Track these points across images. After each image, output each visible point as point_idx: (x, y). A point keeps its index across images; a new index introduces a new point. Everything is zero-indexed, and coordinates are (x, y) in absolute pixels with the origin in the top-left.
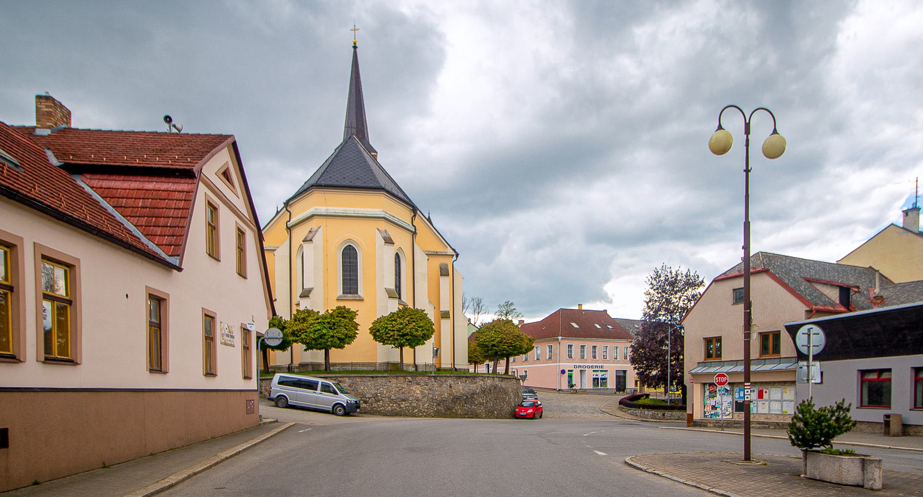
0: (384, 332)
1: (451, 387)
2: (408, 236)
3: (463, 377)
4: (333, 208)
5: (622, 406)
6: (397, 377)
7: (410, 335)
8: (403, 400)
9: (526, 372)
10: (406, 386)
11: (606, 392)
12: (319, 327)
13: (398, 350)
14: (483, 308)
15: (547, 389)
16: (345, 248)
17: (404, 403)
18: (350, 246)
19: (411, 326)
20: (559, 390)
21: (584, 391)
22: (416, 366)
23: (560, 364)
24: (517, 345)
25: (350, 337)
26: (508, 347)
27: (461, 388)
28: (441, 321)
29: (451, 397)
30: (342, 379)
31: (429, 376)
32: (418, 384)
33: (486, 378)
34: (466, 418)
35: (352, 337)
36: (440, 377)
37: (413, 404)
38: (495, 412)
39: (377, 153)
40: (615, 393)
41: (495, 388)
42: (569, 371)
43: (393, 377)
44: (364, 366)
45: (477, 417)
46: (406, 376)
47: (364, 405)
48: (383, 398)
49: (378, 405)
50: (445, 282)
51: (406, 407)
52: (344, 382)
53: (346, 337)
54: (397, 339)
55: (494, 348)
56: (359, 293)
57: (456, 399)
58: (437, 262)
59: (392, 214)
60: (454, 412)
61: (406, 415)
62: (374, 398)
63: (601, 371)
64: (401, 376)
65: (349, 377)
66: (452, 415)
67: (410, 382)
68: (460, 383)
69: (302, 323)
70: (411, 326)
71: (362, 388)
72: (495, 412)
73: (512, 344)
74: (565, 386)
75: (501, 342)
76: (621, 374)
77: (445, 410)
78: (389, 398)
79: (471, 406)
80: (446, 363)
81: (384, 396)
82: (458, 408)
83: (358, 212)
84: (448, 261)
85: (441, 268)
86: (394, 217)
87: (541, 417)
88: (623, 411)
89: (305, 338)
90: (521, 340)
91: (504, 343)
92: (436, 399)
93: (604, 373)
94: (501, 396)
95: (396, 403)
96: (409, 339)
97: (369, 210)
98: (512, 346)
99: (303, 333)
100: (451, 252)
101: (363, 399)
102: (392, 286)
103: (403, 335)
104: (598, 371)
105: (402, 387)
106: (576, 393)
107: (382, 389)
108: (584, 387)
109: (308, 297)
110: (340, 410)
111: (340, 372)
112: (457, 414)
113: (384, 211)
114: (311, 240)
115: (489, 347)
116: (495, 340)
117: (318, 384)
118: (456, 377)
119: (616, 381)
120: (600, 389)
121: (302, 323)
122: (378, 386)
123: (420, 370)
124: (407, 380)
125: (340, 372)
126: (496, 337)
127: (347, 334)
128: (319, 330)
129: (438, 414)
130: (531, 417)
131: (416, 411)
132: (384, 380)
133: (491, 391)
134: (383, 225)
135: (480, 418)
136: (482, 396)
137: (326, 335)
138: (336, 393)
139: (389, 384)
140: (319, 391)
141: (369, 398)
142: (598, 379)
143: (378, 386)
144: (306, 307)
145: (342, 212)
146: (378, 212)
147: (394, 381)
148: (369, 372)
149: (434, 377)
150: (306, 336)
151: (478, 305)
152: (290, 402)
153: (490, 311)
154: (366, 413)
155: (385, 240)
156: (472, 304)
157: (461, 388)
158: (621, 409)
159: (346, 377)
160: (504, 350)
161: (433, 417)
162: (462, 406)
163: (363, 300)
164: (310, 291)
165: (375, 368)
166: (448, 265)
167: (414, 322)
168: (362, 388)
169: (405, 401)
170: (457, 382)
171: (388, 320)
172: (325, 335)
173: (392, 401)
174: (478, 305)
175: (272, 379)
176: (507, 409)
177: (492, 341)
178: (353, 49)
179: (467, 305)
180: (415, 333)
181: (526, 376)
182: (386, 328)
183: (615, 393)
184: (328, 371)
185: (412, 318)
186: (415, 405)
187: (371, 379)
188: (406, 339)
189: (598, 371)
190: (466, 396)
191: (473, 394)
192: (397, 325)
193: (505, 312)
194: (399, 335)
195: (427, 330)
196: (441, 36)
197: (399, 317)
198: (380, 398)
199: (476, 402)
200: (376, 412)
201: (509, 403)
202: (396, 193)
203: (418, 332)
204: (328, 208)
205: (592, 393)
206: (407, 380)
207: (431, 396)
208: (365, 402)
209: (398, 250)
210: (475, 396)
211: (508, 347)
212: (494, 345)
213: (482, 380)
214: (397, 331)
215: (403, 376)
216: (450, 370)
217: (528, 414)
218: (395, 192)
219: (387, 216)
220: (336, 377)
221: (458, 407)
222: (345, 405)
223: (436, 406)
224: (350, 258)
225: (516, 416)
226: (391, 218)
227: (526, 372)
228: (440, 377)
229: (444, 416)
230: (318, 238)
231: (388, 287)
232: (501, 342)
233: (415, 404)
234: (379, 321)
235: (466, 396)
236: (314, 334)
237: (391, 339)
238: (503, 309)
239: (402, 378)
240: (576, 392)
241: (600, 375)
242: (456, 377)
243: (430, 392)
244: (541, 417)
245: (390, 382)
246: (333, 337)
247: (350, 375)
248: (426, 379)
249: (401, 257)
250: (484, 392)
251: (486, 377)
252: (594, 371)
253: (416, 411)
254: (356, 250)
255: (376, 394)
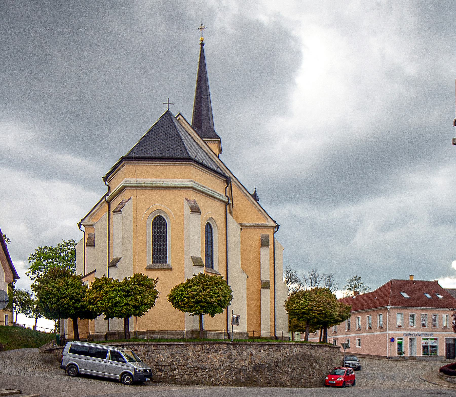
0: (180, 299)
1: (252, 355)
2: (221, 208)
3: (266, 345)
4: (143, 179)
5: (442, 374)
6: (194, 345)
7: (205, 302)
8: (200, 369)
9: (348, 341)
10: (202, 354)
11: (436, 359)
12: (112, 295)
13: (198, 317)
14: (334, 283)
15: (377, 356)
16: (155, 218)
17: (200, 371)
18: (159, 216)
19: (205, 292)
20: (389, 358)
21: (413, 359)
22: (228, 335)
23: (390, 332)
24: (327, 312)
25: (146, 304)
26: (318, 314)
27: (263, 356)
28: (262, 290)
29: (252, 365)
30: (138, 347)
31: (228, 344)
32: (216, 352)
33: (293, 346)
34: (268, 386)
35: (152, 304)
36: (240, 344)
37: (210, 372)
38: (303, 380)
39: (220, 138)
40: (445, 360)
41: (303, 355)
42: (399, 339)
43: (190, 345)
44: (172, 334)
45: (281, 385)
46: (203, 344)
47: (159, 374)
48: (179, 367)
49: (174, 373)
50: (266, 253)
51: (203, 375)
52: (140, 350)
53: (142, 305)
54: (192, 307)
55: (305, 316)
56: (168, 263)
57: (258, 367)
58: (257, 234)
59: (202, 185)
60: (255, 381)
61: (203, 384)
62: (170, 366)
63: (431, 339)
64: (198, 344)
65: (145, 345)
66: (253, 384)
67: (208, 350)
68: (262, 351)
69: (99, 290)
70: (205, 292)
71: (158, 356)
72: (303, 380)
73: (322, 311)
74: (395, 354)
75: (311, 310)
76: (451, 342)
77: (245, 379)
78: (186, 366)
79: (275, 374)
80: (266, 332)
81: (181, 364)
82: (260, 377)
83: (167, 183)
84: (269, 232)
85: (262, 239)
86: (204, 187)
87: (353, 385)
88: (443, 379)
89: (99, 306)
90: (331, 307)
91: (315, 310)
92: (236, 368)
93: (434, 341)
94: (311, 364)
95: (192, 371)
96: (204, 307)
97: (177, 180)
98: (322, 313)
99: (98, 301)
100: (271, 224)
101: (158, 367)
102: (200, 254)
103: (198, 302)
104: (427, 339)
105: (199, 355)
106: (404, 360)
107: (178, 357)
108: (413, 355)
109: (116, 266)
110: (128, 380)
111: (148, 340)
112: (258, 382)
113: (192, 181)
114: (120, 211)
115: (299, 314)
116: (305, 307)
117: (107, 352)
118: (258, 345)
119: (447, 349)
120: (430, 356)
121: (99, 290)
122: (174, 354)
123: (233, 337)
124: (204, 348)
125: (148, 340)
126: (306, 305)
127: (142, 302)
128: (112, 297)
129: (237, 383)
130: (342, 385)
131: (213, 379)
132: (180, 348)
133: (297, 359)
134: (192, 195)
135: (284, 386)
136: (286, 364)
137: (119, 303)
138: (125, 362)
139: (185, 352)
140: (107, 360)
141: (165, 366)
142: (427, 347)
143: (174, 354)
144: (104, 275)
145: (151, 183)
146: (186, 182)
147: (191, 348)
148: (177, 340)
149: (233, 344)
150: (101, 304)
151: (329, 280)
152: (80, 370)
153: (340, 287)
154: (162, 381)
155: (191, 209)
156: (323, 279)
157: (263, 356)
158: (440, 377)
159: (142, 345)
160: (314, 318)
161: (231, 385)
162: (265, 374)
163: (171, 269)
164: (118, 260)
165: (182, 336)
166: (268, 236)
167: (208, 288)
168: (158, 356)
169: (202, 369)
170: (259, 350)
171: (184, 287)
172: (118, 302)
173: (188, 369)
174: (329, 280)
175: (64, 348)
176: (316, 377)
177: (302, 309)
178: (200, 46)
179: (319, 280)
180: (209, 300)
181: (347, 344)
182: (182, 295)
183: (445, 360)
184: (128, 339)
185: (207, 285)
186: (212, 373)
187: (167, 347)
188: (201, 306)
189: (427, 339)
190: (269, 364)
191: (277, 362)
192: (192, 291)
193: (353, 286)
194: (194, 302)
195: (223, 296)
196: (296, 39)
197: (194, 284)
198: (176, 366)
199: (280, 370)
200: (172, 381)
201: (320, 371)
202: (208, 165)
203: (212, 298)
204: (138, 179)
205: (421, 360)
206: (204, 348)
207: (229, 364)
208: (161, 371)
209: (209, 220)
210: (279, 365)
211: (318, 314)
212: (304, 313)
213: (287, 348)
214: (192, 297)
215: (200, 344)
216: (271, 338)
217: (337, 382)
218: (213, 167)
219: (195, 186)
220: (132, 345)
221: (260, 376)
222: (133, 374)
223: (235, 375)
224: (160, 228)
225: (326, 384)
226: (200, 188)
227: (348, 341)
228: (240, 344)
229: (244, 384)
230: (127, 209)
231: (194, 255)
232: (311, 310)
233: (213, 372)
234: (177, 288)
235: (269, 364)
236: (108, 302)
237: (186, 306)
238: (352, 283)
239: (199, 346)
240: (404, 359)
241: (430, 343)
242: (258, 345)
243: (228, 360)
244: (353, 385)
245: (187, 350)
246: (127, 304)
247: (146, 343)
248: (224, 347)
249: (213, 228)
250: (289, 359)
251: (292, 345)
252: (424, 339)
253: (213, 379)
254: (165, 220)
255: (172, 362)
